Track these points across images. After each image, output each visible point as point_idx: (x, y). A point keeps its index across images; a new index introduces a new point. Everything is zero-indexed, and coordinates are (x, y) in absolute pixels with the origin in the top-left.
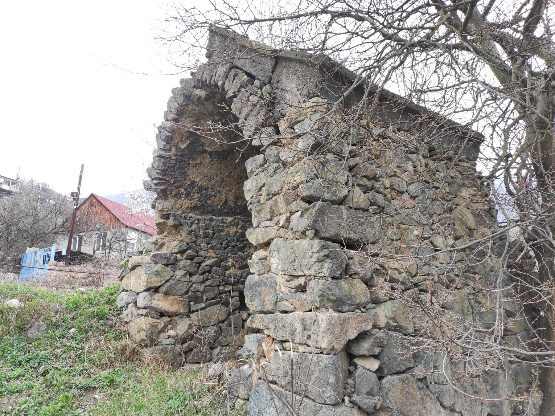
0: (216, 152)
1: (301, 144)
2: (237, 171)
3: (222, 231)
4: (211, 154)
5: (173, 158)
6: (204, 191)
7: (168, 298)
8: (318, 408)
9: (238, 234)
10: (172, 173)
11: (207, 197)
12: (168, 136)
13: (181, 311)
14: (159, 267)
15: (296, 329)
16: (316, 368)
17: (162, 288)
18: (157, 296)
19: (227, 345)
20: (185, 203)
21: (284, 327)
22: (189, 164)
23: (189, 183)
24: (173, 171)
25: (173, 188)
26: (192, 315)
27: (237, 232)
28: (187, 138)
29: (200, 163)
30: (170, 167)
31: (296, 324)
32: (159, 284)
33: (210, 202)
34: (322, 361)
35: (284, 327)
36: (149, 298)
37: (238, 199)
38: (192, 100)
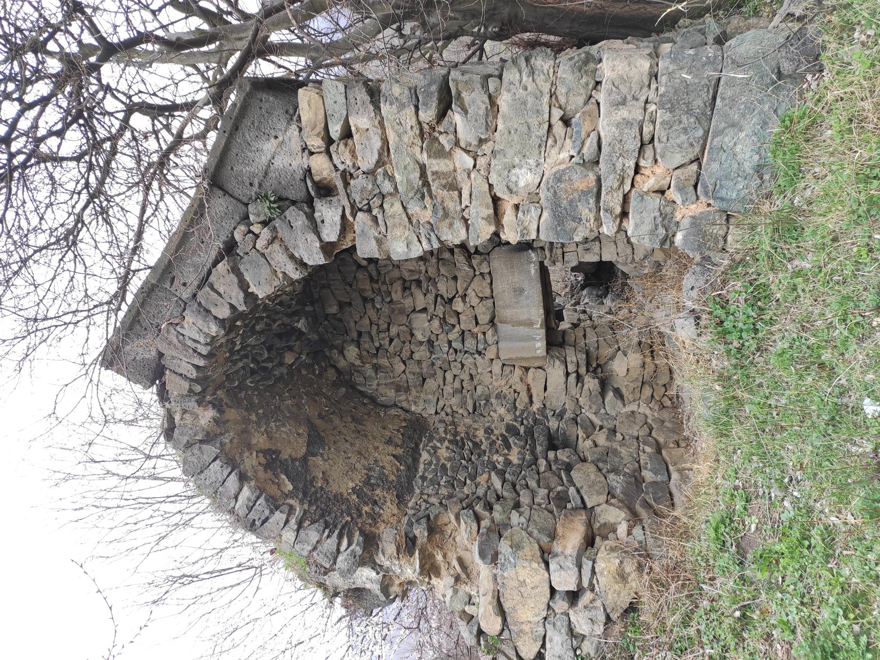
0: (308, 445)
1: (361, 121)
2: (344, 431)
5: (306, 506)
6: (372, 481)
7: (560, 534)
8: (730, 61)
9: (451, 447)
10: (333, 515)
11: (383, 478)
12: (267, 500)
14: (504, 547)
15: (624, 119)
17: (542, 543)
18: (557, 548)
19: (638, 462)
20: (389, 509)
21: (621, 140)
22: (322, 488)
23: (354, 497)
24: (330, 514)
26: (589, 505)
27: (447, 448)
28: (277, 476)
29: (323, 473)
30: (322, 516)
31: (618, 118)
32: (536, 547)
33: (392, 478)
34: (668, 68)
35: (621, 140)
36: (561, 558)
38: (216, 435)
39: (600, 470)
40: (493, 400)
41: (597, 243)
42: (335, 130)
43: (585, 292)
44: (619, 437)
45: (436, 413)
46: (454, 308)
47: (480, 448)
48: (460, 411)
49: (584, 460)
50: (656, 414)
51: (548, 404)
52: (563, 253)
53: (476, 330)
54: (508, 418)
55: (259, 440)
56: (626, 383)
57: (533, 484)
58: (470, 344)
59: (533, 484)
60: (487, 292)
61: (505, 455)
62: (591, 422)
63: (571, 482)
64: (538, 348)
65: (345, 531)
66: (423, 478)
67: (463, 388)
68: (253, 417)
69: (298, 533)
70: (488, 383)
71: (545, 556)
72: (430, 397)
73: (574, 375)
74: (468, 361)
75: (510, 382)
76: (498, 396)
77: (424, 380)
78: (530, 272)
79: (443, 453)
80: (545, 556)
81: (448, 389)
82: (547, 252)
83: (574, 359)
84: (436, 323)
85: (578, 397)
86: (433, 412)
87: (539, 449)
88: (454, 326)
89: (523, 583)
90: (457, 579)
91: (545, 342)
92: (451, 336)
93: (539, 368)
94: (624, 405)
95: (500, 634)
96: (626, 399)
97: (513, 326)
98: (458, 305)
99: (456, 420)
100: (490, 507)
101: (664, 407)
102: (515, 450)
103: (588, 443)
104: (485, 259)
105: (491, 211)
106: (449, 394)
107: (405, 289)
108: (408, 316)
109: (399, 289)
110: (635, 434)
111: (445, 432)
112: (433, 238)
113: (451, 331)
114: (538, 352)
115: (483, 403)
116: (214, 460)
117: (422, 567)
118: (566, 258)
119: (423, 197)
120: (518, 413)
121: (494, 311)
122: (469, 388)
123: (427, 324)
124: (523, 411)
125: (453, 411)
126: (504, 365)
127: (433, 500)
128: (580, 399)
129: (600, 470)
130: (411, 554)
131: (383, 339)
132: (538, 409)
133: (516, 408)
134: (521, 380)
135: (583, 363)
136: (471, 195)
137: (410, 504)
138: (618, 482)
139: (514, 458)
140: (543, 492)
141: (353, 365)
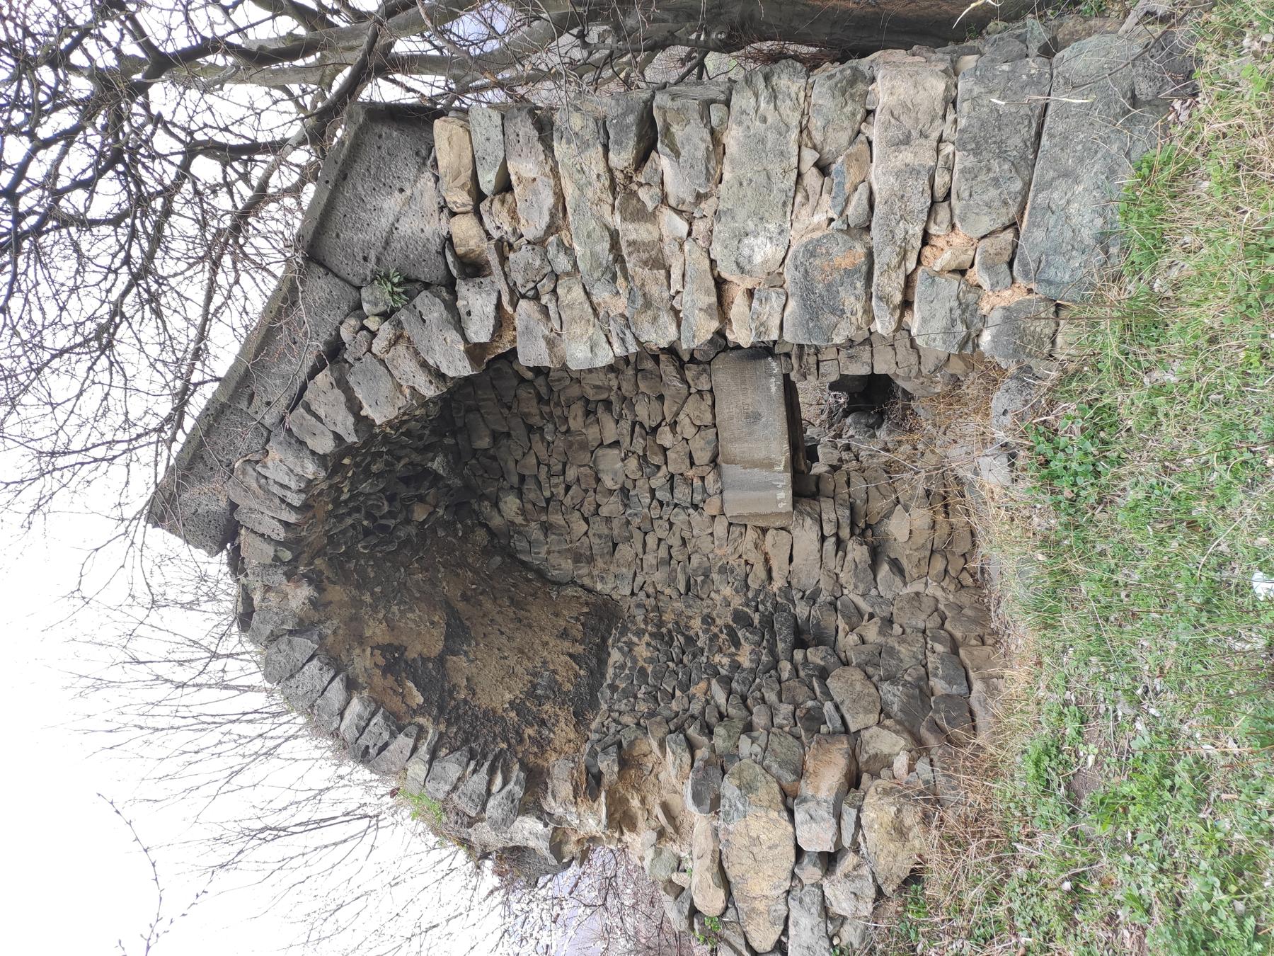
0: (446, 639)
2: (499, 619)
4: (449, 650)
5: (442, 727)
6: (539, 692)
7: (811, 770)
10: (482, 741)
11: (554, 686)
13: (846, 746)
16: (985, 102)
17: (784, 783)
18: (806, 789)
19: (925, 666)
20: (563, 732)
21: (903, 196)
22: (465, 701)
23: (513, 714)
25: (519, 749)
26: (853, 729)
30: (466, 741)
32: (776, 788)
34: (971, 91)
35: (903, 196)
37: (567, 635)
38: (312, 624)
39: (869, 677)
40: (715, 576)
41: (867, 348)
43: (849, 420)
44: (897, 629)
45: (633, 594)
46: (658, 442)
47: (695, 645)
48: (667, 591)
49: (846, 663)
50: (951, 597)
51: (794, 582)
52: (818, 362)
53: (690, 473)
54: (737, 602)
55: (376, 631)
56: (908, 552)
57: (771, 697)
59: (771, 697)
60: (708, 418)
61: (731, 655)
62: (857, 608)
63: (827, 694)
64: (781, 501)
65: (499, 764)
66: (613, 688)
67: (671, 557)
68: (367, 598)
69: (430, 765)
70: (707, 551)
71: (789, 802)
72: (624, 570)
73: (833, 539)
74: (680, 518)
75: (740, 549)
76: (722, 570)
77: (615, 545)
78: (769, 389)
79: (642, 651)
80: (789, 802)
81: (650, 559)
82: (794, 360)
83: (833, 516)
84: (633, 463)
85: (837, 571)
86: (628, 592)
87: (781, 646)
88: (658, 467)
90: (661, 834)
91: (790, 492)
93: (782, 529)
94: (905, 584)
95: (723, 914)
96: (907, 575)
97: (745, 468)
98: (665, 438)
99: (661, 604)
100: (708, 731)
101: (963, 586)
102: (746, 648)
103: (853, 638)
104: (704, 370)
105: (714, 299)
106: (651, 566)
107: (588, 413)
108: (592, 452)
109: (580, 413)
110: (921, 625)
111: (645, 621)
113: (654, 474)
114: (781, 505)
115: (700, 579)
116: (310, 659)
117: (610, 816)
118: (822, 370)
120: (750, 595)
121: (717, 446)
122: (680, 558)
123: (620, 464)
124: (758, 592)
125: (657, 592)
126: (730, 524)
127: (627, 719)
128: (841, 575)
129: (869, 677)
130: (595, 798)
131: (556, 486)
132: (780, 589)
133: (748, 587)
135: (845, 523)
136: (684, 276)
137: (594, 726)
138: (895, 695)
139: (745, 660)
140: (786, 709)
141: (513, 523)
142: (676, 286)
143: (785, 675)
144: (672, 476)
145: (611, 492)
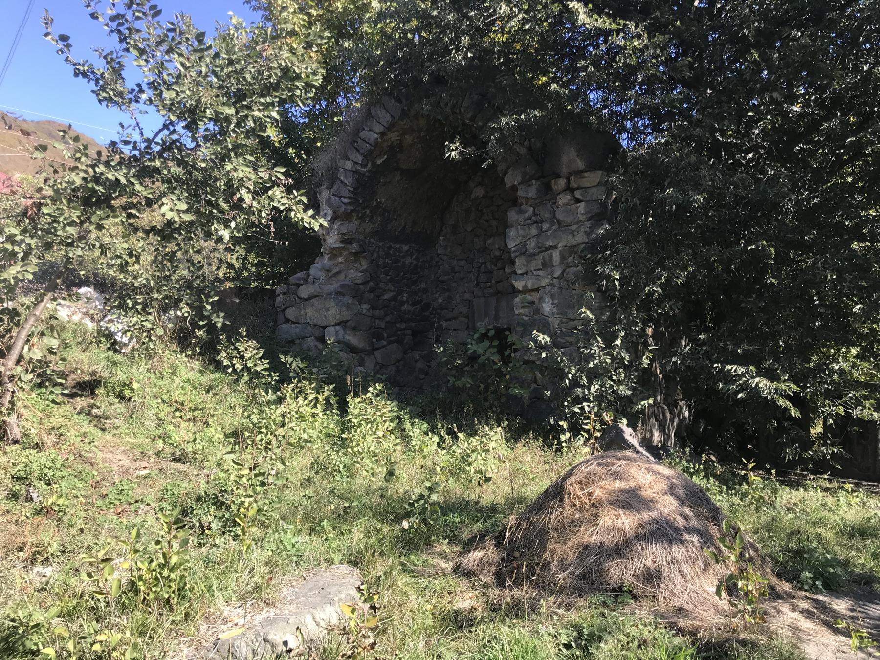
3: (399, 261)
5: (367, 174)
26: (376, 353)
39: (398, 361)
40: (447, 294)
42: (578, 194)
44: (422, 377)
45: (438, 255)
48: (439, 272)
49: (405, 353)
55: (408, 139)
57: (388, 318)
58: (483, 278)
59: (388, 318)
61: (407, 302)
63: (389, 343)
65: (354, 201)
66: (390, 248)
68: (423, 134)
71: (342, 323)
76: (450, 298)
77: (461, 245)
79: (408, 261)
80: (342, 323)
81: (455, 263)
84: (497, 253)
86: (439, 252)
87: (413, 324)
88: (496, 266)
89: (327, 310)
90: (328, 271)
92: (488, 264)
95: (66, 651)
100: (372, 291)
102: (412, 309)
105: (530, 288)
112: (517, 254)
115: (445, 287)
117: (334, 249)
119: (539, 248)
127: (375, 255)
129: (398, 361)
133: (442, 310)
134: (461, 313)
137: (372, 240)
139: (405, 307)
140: (383, 325)
141: (471, 193)
142: (534, 272)
143: (398, 325)
144: (492, 272)
145: (485, 243)
